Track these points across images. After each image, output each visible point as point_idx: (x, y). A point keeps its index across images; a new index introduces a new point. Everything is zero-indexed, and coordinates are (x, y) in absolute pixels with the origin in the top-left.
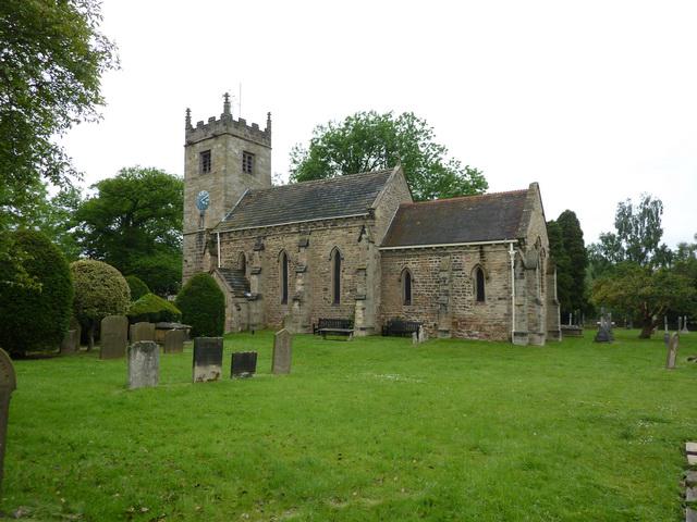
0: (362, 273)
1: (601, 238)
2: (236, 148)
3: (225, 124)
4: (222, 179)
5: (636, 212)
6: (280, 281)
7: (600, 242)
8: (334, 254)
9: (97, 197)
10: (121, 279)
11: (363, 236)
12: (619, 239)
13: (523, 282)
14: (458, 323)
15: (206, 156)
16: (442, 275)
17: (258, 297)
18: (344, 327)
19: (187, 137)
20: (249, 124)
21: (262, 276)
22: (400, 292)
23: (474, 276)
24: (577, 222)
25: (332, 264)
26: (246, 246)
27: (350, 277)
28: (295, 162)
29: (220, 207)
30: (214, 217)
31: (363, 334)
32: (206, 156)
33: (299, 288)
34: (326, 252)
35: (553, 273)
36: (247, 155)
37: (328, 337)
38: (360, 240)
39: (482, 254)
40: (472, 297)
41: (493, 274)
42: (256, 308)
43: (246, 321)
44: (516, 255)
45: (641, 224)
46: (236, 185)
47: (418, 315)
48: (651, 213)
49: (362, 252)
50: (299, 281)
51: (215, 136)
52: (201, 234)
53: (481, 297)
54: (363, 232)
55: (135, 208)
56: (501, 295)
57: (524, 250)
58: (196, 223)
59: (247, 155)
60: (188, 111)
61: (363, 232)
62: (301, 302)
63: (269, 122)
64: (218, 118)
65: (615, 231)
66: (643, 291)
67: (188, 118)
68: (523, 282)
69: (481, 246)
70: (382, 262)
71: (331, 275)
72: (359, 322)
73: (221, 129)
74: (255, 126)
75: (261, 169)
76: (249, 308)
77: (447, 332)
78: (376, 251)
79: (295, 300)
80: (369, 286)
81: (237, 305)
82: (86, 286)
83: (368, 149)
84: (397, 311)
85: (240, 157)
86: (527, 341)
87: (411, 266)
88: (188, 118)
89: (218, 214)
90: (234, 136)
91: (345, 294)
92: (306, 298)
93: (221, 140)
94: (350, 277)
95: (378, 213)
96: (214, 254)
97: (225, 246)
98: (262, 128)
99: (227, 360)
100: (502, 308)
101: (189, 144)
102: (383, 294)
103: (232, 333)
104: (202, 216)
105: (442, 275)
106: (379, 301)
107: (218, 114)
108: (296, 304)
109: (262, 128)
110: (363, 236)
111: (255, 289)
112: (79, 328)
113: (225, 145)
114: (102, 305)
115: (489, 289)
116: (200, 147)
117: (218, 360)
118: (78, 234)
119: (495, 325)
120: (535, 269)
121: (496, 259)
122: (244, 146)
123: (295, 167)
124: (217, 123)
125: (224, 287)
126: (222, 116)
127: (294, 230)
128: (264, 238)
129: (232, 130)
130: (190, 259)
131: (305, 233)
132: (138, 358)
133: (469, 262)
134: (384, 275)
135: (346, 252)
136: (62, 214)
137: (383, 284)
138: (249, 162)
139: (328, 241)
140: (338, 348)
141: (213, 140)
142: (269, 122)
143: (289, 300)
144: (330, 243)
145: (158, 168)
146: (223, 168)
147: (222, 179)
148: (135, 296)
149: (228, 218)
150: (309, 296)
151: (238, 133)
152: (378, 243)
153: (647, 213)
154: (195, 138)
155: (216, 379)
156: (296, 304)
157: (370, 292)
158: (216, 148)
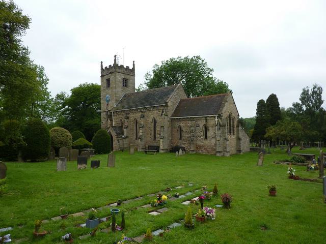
0: (162, 128)
1: (293, 105)
2: (119, 77)
3: (115, 68)
4: (114, 90)
5: (310, 92)
6: (135, 131)
7: (293, 107)
10: (69, 134)
12: (302, 105)
13: (220, 132)
14: (198, 147)
15: (108, 80)
16: (192, 128)
17: (127, 137)
18: (157, 149)
19: (101, 73)
20: (125, 67)
21: (128, 129)
22: (177, 135)
23: (204, 129)
24: (277, 99)
25: (153, 124)
26: (122, 117)
27: (159, 129)
28: (147, 80)
29: (114, 101)
31: (162, 151)
32: (108, 80)
33: (141, 134)
34: (150, 120)
35: (239, 127)
37: (147, 153)
38: (162, 115)
39: (206, 120)
40: (203, 137)
41: (210, 128)
42: (126, 141)
43: (122, 147)
44: (218, 121)
45: (311, 97)
46: (120, 92)
47: (184, 144)
48: (273, 99)
49: (164, 121)
50: (141, 131)
51: (111, 73)
53: (206, 137)
54: (163, 112)
55: (86, 99)
56: (213, 136)
57: (221, 119)
60: (102, 62)
61: (163, 112)
62: (141, 139)
63: (134, 65)
64: (112, 66)
65: (300, 102)
66: (282, 133)
67: (102, 66)
68: (220, 132)
69: (206, 117)
70: (171, 123)
71: (153, 129)
72: (161, 147)
73: (113, 70)
74: (128, 67)
75: (131, 85)
76: (123, 141)
77: (193, 151)
78: (168, 119)
79: (139, 138)
80: (166, 133)
81: (118, 140)
82: (56, 137)
84: (178, 143)
85: (122, 81)
86: (222, 155)
87: (182, 125)
88: (102, 66)
91: (157, 136)
92: (143, 138)
93: (114, 74)
94: (159, 129)
95: (169, 104)
96: (111, 120)
97: (115, 117)
99: (89, 162)
100: (213, 141)
101: (102, 76)
102: (172, 135)
103: (116, 151)
104: (107, 105)
105: (192, 128)
106: (170, 139)
108: (140, 140)
111: (125, 134)
112: (54, 151)
113: (115, 76)
114: (61, 143)
115: (209, 134)
117: (86, 163)
118: (65, 110)
120: (225, 126)
121: (211, 122)
122: (123, 76)
123: (147, 81)
124: (112, 67)
125: (114, 134)
126: (114, 65)
127: (139, 111)
129: (118, 70)
130: (104, 122)
131: (143, 112)
132: (60, 162)
133: (202, 123)
134: (172, 128)
135: (158, 119)
136: (59, 103)
137: (171, 132)
138: (125, 82)
139: (152, 115)
140: (155, 157)
142: (134, 65)
145: (94, 83)
146: (114, 86)
147: (114, 90)
148: (74, 139)
149: (117, 106)
150: (145, 137)
151: (120, 71)
152: (169, 115)
153: (314, 92)
154: (105, 73)
156: (140, 140)
157: (166, 135)
158: (112, 77)
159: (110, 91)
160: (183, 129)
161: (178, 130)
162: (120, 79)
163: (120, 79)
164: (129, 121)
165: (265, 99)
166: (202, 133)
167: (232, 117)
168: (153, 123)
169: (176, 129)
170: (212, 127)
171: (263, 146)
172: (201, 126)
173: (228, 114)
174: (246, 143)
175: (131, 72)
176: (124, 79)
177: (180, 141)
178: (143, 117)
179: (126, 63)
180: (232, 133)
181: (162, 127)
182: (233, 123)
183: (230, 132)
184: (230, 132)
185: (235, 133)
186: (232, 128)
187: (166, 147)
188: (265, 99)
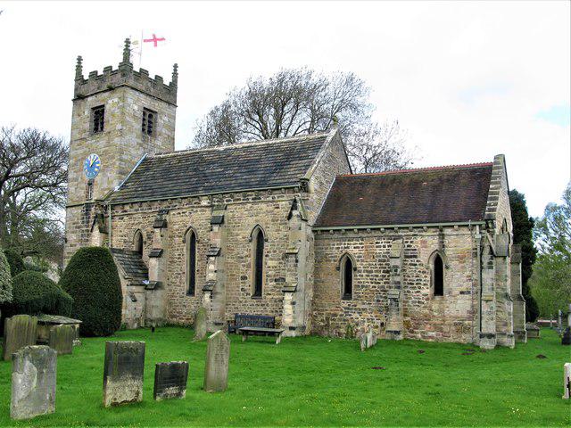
2: (135, 103)
3: (124, 75)
8: (255, 234)
11: (295, 213)
15: (99, 113)
17: (158, 286)
19: (76, 90)
20: (152, 76)
22: (337, 283)
23: (432, 266)
25: (253, 246)
29: (112, 174)
30: (105, 186)
33: (211, 276)
34: (244, 232)
36: (148, 113)
38: (290, 217)
41: (453, 264)
50: (212, 267)
51: (111, 89)
52: (88, 206)
53: (439, 290)
54: (294, 207)
58: (82, 193)
59: (148, 113)
61: (294, 207)
63: (175, 74)
67: (79, 68)
71: (252, 260)
73: (118, 79)
80: (300, 276)
85: (140, 114)
87: (352, 251)
88: (79, 68)
90: (132, 88)
91: (268, 285)
92: (218, 289)
93: (119, 93)
95: (313, 185)
98: (167, 81)
101: (79, 98)
107: (115, 62)
108: (207, 295)
109: (167, 81)
110: (295, 213)
111: (154, 275)
113: (123, 99)
116: (92, 102)
119: (456, 324)
134: (318, 262)
135: (270, 233)
138: (149, 122)
139: (247, 215)
142: (175, 74)
144: (252, 221)
146: (119, 126)
147: (117, 140)
149: (123, 187)
158: (111, 103)
161: (338, 269)
162: (136, 108)
163: (136, 108)
164: (166, 236)
168: (255, 240)
169: (332, 265)
170: (461, 259)
175: (167, 93)
177: (345, 304)
179: (152, 62)
181: (287, 255)
187: (300, 321)
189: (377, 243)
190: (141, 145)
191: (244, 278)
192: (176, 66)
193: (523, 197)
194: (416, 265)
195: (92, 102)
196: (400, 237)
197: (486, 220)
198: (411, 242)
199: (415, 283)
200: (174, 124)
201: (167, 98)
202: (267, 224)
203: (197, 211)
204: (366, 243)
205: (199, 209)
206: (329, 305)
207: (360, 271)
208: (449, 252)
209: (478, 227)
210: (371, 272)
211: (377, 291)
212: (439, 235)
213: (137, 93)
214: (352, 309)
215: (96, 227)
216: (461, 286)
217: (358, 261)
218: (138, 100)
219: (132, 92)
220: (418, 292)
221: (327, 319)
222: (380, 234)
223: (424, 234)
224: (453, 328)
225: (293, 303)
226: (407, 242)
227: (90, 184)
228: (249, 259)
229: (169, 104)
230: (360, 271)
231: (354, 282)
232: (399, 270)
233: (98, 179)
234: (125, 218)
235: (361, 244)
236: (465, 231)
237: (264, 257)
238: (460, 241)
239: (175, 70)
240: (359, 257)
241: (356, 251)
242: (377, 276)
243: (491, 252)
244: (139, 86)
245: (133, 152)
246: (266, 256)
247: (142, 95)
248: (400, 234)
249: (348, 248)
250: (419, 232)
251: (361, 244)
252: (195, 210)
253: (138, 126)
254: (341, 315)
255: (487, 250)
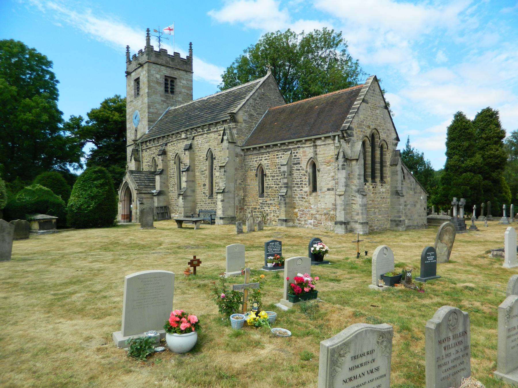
0: (223, 170)
9: (402, 152)
23: (310, 170)
25: (207, 163)
34: (201, 154)
40: (307, 189)
59: (170, 80)
61: (224, 134)
63: (191, 50)
64: (143, 51)
67: (128, 53)
71: (207, 173)
72: (219, 213)
83: (19, 42)
85: (162, 81)
87: (264, 162)
88: (128, 53)
89: (144, 128)
90: (154, 63)
101: (128, 74)
109: (184, 55)
116: (134, 76)
126: (146, 47)
128: (166, 145)
135: (217, 153)
141: (140, 69)
142: (191, 50)
143: (214, 194)
144: (206, 146)
155: (418, 291)
159: (140, 102)
160: (267, 172)
161: (256, 175)
165: (471, 117)
166: (306, 179)
167: (378, 142)
168: (209, 159)
171: (458, 210)
172: (304, 163)
173: (368, 132)
174: (418, 206)
176: (166, 78)
178: (190, 148)
180: (378, 180)
182: (382, 154)
183: (373, 177)
184: (373, 177)
185: (388, 179)
186: (378, 166)
188: (471, 117)
189: (277, 155)
190: (165, 102)
191: (204, 185)
192: (191, 44)
193: (497, 113)
194: (299, 170)
195: (134, 76)
196: (290, 149)
197: (342, 131)
198: (297, 153)
199: (299, 183)
200: (192, 85)
201: (185, 67)
202: (214, 147)
203: (180, 143)
204: (271, 156)
205: (181, 141)
206: (253, 201)
207: (268, 177)
208: (320, 159)
209: (337, 137)
210: (274, 176)
211: (278, 190)
212: (313, 146)
213: (159, 66)
214: (264, 204)
215: (133, 158)
216: (328, 184)
217: (267, 169)
218: (160, 71)
219: (154, 66)
220: (301, 190)
221: (252, 211)
222: (279, 149)
223: (304, 146)
224: (323, 217)
225: (222, 201)
226: (294, 153)
227: (136, 130)
228: (206, 172)
229: (186, 71)
230: (268, 177)
231: (265, 185)
232: (286, 174)
233: (139, 127)
234: (148, 150)
235: (268, 156)
236: (330, 141)
237: (214, 170)
238: (327, 150)
239: (191, 47)
240: (268, 166)
241: (266, 162)
242: (277, 179)
243: (344, 156)
244: (160, 61)
245: (158, 106)
246: (215, 169)
247: (162, 67)
248: (290, 147)
249: (261, 160)
250: (301, 144)
251: (268, 156)
252: (179, 141)
253: (162, 89)
254: (259, 208)
255: (341, 155)
